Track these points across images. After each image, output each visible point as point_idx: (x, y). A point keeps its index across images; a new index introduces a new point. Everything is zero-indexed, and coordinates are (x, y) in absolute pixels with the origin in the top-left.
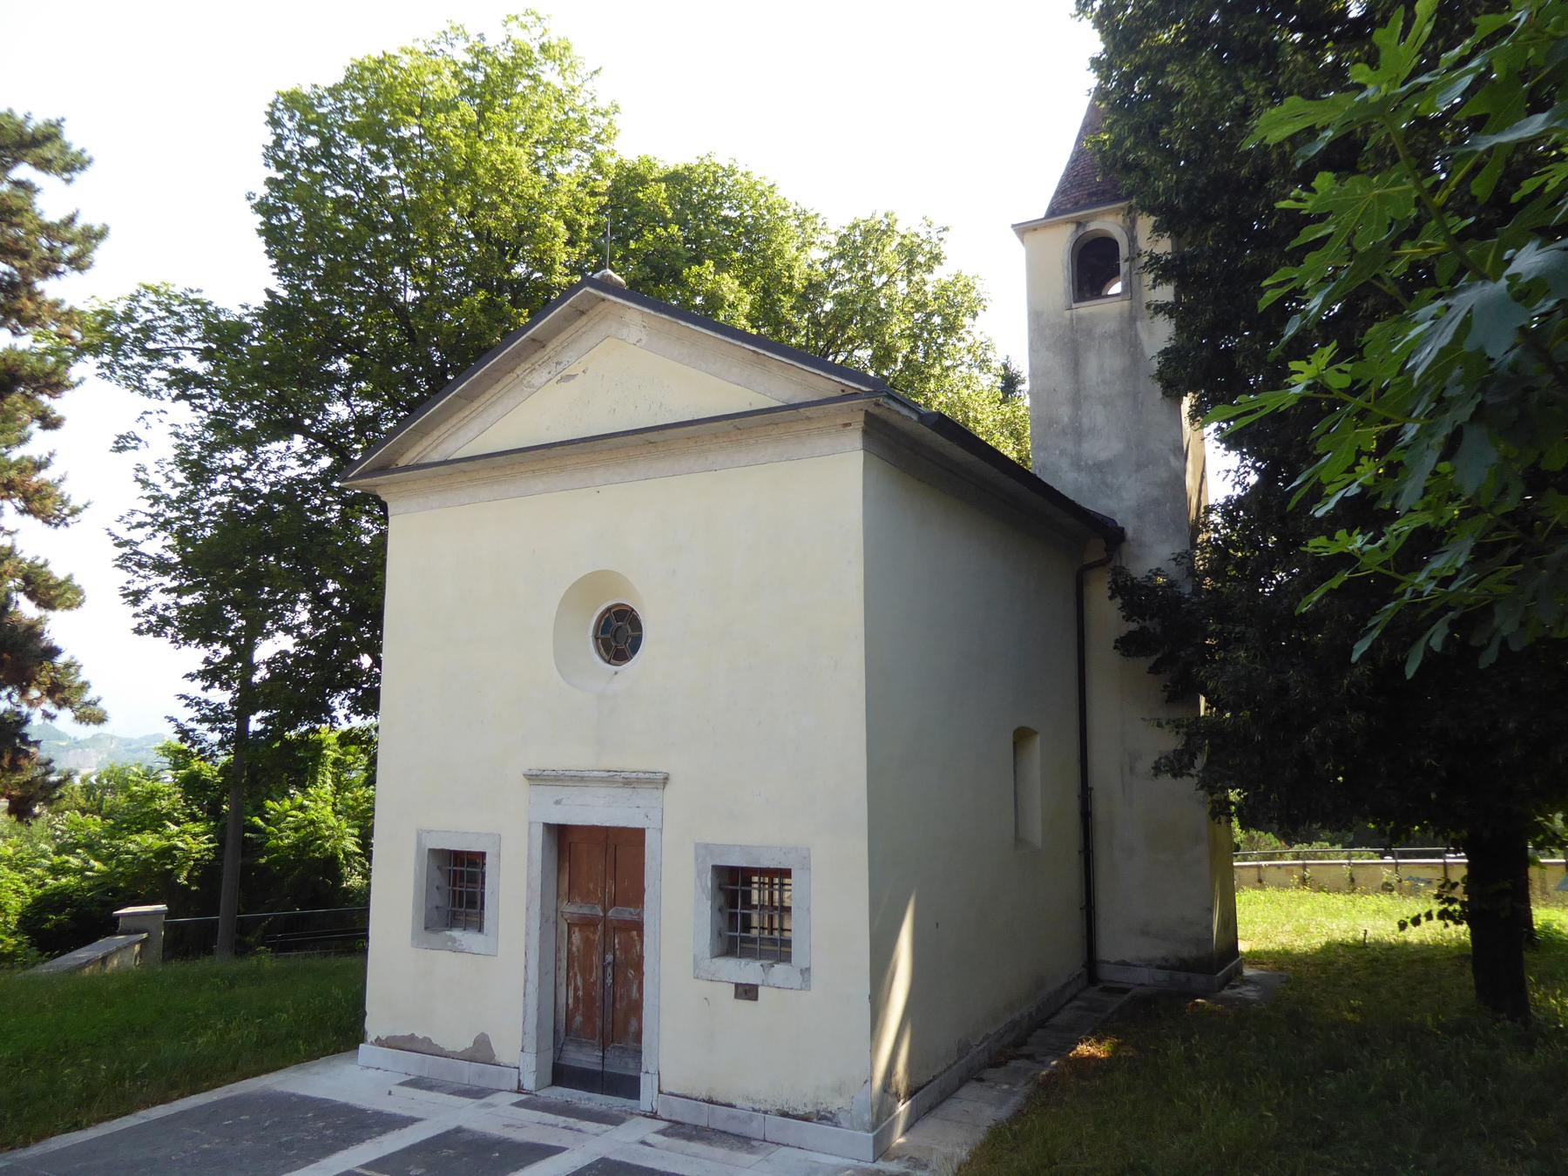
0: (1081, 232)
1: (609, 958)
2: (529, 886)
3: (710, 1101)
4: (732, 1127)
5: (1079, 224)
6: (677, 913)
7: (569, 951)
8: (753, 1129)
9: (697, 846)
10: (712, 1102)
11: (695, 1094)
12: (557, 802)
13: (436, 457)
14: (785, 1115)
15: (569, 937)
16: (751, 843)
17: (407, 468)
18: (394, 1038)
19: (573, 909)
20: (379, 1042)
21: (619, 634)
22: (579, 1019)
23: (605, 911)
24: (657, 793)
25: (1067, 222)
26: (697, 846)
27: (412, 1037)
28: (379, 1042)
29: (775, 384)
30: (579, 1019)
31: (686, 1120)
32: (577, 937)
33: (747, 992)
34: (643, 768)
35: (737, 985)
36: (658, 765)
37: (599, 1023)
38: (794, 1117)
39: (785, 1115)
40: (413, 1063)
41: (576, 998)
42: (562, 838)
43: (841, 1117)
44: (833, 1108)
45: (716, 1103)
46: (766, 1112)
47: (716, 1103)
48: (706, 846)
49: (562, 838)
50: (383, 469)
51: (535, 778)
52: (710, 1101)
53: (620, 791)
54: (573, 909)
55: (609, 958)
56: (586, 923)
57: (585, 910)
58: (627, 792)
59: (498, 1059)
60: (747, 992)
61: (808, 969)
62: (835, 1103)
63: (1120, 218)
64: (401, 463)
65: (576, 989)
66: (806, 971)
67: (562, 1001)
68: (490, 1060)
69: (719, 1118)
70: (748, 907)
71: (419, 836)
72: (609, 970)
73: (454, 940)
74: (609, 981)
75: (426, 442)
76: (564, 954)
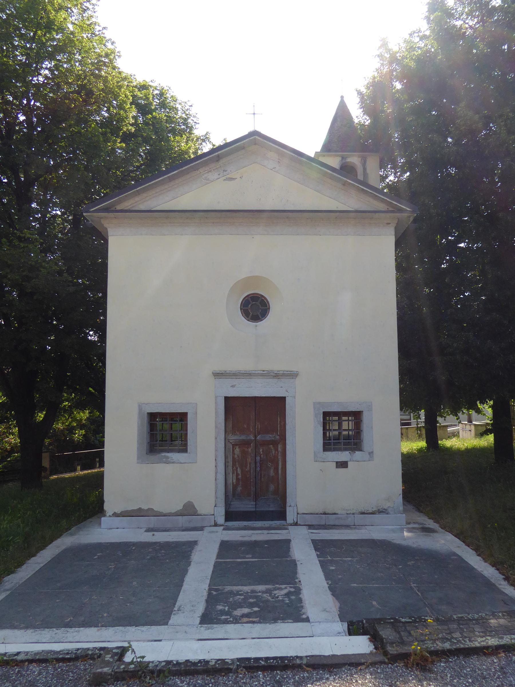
0: (344, 161)
1: (258, 458)
2: (216, 427)
3: (325, 514)
4: (337, 523)
5: (343, 158)
6: (303, 433)
7: (233, 458)
8: (349, 521)
9: (314, 404)
10: (326, 514)
11: (317, 512)
12: (233, 386)
13: (142, 207)
14: (363, 513)
15: (233, 451)
16: (343, 399)
17: (122, 211)
18: (126, 511)
19: (233, 438)
20: (115, 515)
21: (255, 307)
22: (239, 489)
23: (255, 437)
24: (292, 380)
25: (337, 156)
26: (314, 404)
27: (140, 509)
28: (115, 515)
29: (352, 201)
30: (239, 489)
31: (313, 524)
32: (237, 450)
33: (343, 465)
34: (283, 369)
35: (337, 463)
36: (294, 369)
37: (253, 489)
38: (367, 514)
39: (363, 513)
40: (153, 521)
41: (237, 479)
42: (232, 405)
43: (389, 510)
44: (386, 507)
45: (328, 514)
46: (353, 514)
47: (328, 514)
48: (319, 403)
49: (232, 405)
50: (107, 210)
51: (218, 375)
52: (325, 514)
53: (271, 380)
54: (233, 438)
55: (258, 458)
56: (244, 444)
57: (243, 437)
58: (275, 380)
59: (199, 512)
60: (343, 465)
61: (372, 452)
62: (386, 505)
63: (360, 159)
64: (119, 207)
65: (237, 475)
66: (371, 453)
67: (230, 481)
68: (195, 513)
69: (331, 520)
70: (343, 431)
71: (139, 406)
72: (258, 464)
73: (167, 458)
74: (258, 469)
75: (137, 199)
76: (230, 459)
